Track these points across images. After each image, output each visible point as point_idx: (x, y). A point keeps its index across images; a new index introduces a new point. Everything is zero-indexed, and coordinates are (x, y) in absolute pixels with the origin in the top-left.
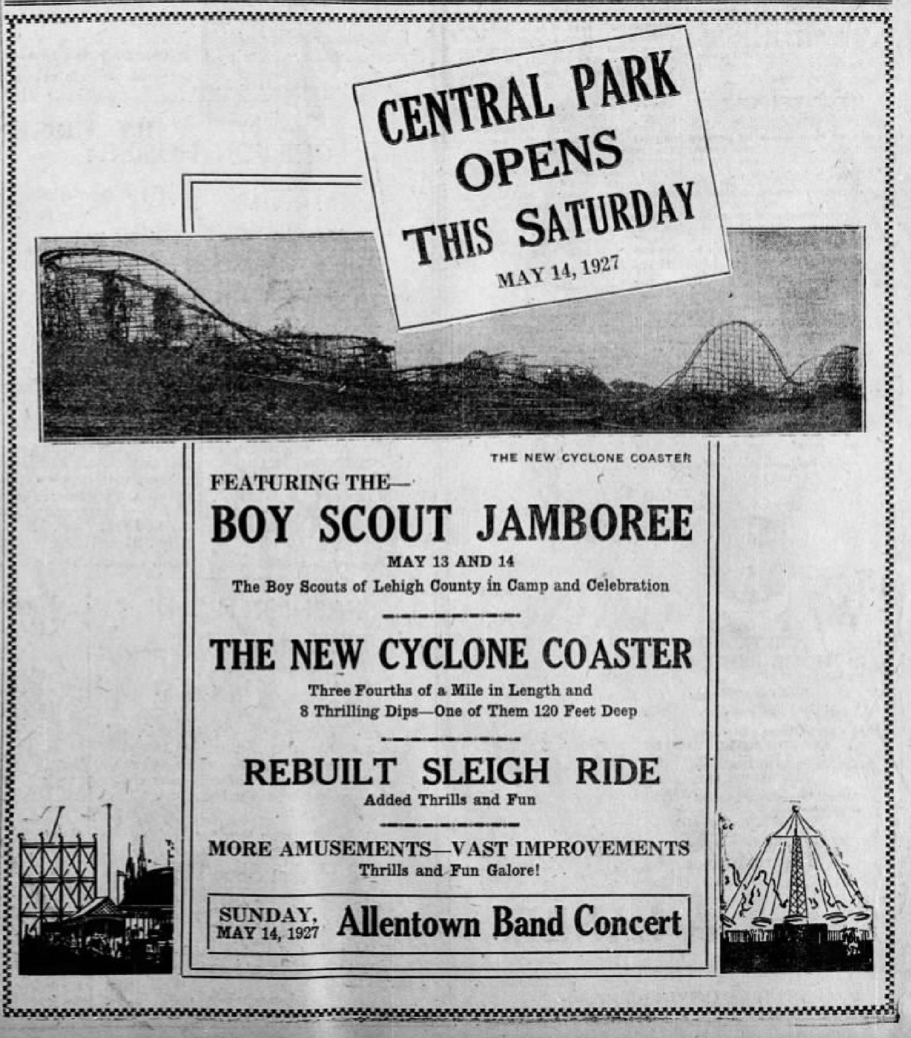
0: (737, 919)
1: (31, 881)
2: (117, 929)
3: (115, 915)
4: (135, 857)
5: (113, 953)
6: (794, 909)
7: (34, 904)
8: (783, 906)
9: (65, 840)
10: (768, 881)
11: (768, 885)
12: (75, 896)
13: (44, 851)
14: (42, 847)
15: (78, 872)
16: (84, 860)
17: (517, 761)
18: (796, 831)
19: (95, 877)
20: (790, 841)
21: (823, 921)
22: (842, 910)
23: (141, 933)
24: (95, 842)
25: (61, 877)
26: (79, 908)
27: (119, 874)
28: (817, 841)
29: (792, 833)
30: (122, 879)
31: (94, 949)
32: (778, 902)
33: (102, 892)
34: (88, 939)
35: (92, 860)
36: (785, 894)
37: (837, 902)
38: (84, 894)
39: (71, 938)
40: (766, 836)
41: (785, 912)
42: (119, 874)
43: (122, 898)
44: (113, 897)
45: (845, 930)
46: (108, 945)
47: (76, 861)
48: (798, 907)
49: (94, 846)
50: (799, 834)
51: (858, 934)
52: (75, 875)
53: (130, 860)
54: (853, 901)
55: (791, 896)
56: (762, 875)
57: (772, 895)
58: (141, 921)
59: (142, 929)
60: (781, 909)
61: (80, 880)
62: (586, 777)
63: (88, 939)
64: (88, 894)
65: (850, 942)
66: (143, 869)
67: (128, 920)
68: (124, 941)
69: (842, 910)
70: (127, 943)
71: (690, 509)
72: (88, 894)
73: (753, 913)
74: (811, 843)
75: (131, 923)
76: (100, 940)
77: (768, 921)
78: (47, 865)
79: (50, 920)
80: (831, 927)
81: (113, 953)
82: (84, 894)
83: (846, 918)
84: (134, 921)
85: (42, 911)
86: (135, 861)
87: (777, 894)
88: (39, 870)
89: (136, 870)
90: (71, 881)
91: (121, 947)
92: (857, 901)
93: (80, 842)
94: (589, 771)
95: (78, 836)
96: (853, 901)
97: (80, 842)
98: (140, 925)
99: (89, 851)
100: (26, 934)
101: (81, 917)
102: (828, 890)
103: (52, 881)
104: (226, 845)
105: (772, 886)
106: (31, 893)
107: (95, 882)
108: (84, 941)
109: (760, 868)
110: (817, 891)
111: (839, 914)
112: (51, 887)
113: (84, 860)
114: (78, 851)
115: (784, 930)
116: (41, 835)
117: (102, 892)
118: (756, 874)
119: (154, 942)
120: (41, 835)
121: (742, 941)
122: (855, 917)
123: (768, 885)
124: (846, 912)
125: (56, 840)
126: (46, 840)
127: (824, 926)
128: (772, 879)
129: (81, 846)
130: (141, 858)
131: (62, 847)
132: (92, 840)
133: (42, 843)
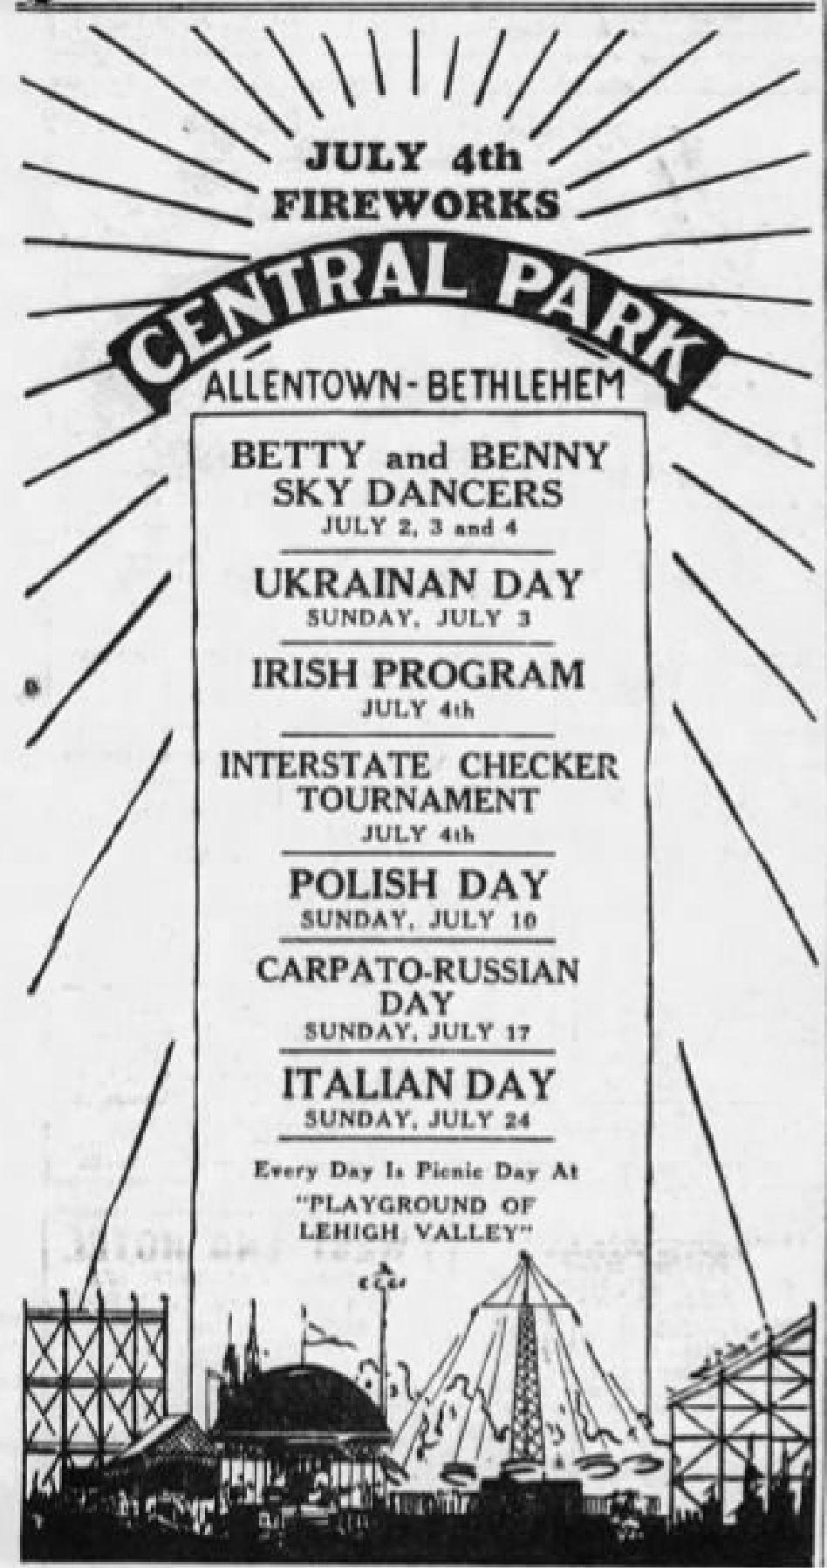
0: (413, 1466)
1: (44, 1383)
2: (206, 1483)
3: (201, 1454)
4: (240, 1341)
5: (197, 1528)
6: (519, 1445)
7: (50, 1427)
8: (500, 1437)
9: (107, 1306)
10: (470, 1391)
11: (471, 1399)
12: (127, 1412)
13: (68, 1328)
14: (66, 1319)
15: (133, 1370)
16: (143, 1346)
17: (480, 664)
18: (525, 1294)
19: (164, 1379)
20: (513, 1315)
21: (570, 1472)
22: (612, 1448)
23: (249, 1493)
24: (165, 1312)
25: (100, 1376)
26: (136, 1436)
27: (209, 1373)
28: (564, 1315)
29: (518, 1299)
30: (215, 1384)
31: (161, 1519)
32: (489, 1432)
33: (178, 1405)
34: (151, 1502)
35: (159, 1348)
36: (502, 1417)
37: (600, 1432)
38: (142, 1409)
39: (118, 1500)
40: (472, 1305)
41: (501, 1451)
42: (209, 1373)
43: (214, 1416)
44: (199, 1416)
45: (615, 1494)
46: (188, 1514)
47: (128, 1350)
48: (528, 1440)
49: (163, 1319)
50: (531, 1301)
51: (641, 1504)
52: (127, 1375)
53: (231, 1349)
54: (632, 1432)
55: (514, 1418)
56: (460, 1384)
57: (477, 1417)
58: (249, 1466)
59: (253, 1486)
60: (498, 1445)
61: (136, 1384)
62: (411, 680)
63: (151, 1502)
64: (152, 1409)
65: (623, 1518)
66: (253, 1367)
67: (225, 1465)
68: (217, 1506)
69: (612, 1448)
70: (224, 1510)
71: (426, 755)
72: (152, 1409)
73: (439, 1457)
74: (553, 1316)
75: (236, 1471)
76: (171, 1506)
77: (469, 1471)
78: (73, 1354)
79: (82, 1461)
80: (591, 1488)
81: (197, 1528)
82: (142, 1409)
83: (617, 1468)
84: (237, 1465)
85: (65, 1441)
86: (240, 1352)
87: (488, 1415)
88: (59, 1365)
89: (242, 1368)
90: (118, 1384)
91: (212, 1517)
92: (641, 1432)
93: (135, 1311)
94: (528, 495)
95: (134, 1298)
96: (632, 1432)
97: (135, 1311)
98: (248, 1477)
99: (153, 1329)
100: (35, 1489)
101: (138, 1456)
102: (584, 1410)
103: (84, 1384)
104: (521, 1208)
105: (478, 1401)
106: (83, 1403)
107: (163, 1389)
108: (142, 1506)
109: (456, 1371)
110: (563, 1409)
111: (603, 1459)
112: (82, 1395)
113: (143, 1346)
114: (134, 1329)
115: (501, 1486)
116: (64, 1293)
117: (178, 1405)
118: (449, 1382)
119: (274, 1510)
120: (64, 1293)
121: (420, 1512)
122: (633, 1465)
123: (471, 1399)
124: (617, 1454)
125: (92, 1306)
126: (74, 1303)
127: (576, 1485)
128: (479, 1390)
129: (136, 1317)
130: (252, 1346)
131: (102, 1318)
132: (159, 1306)
133: (66, 1310)
